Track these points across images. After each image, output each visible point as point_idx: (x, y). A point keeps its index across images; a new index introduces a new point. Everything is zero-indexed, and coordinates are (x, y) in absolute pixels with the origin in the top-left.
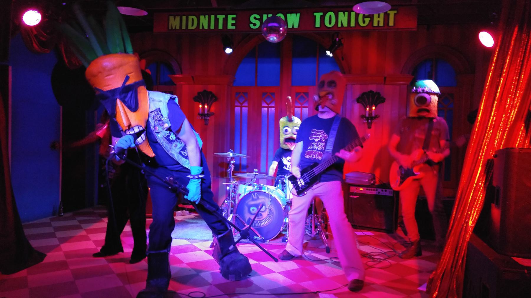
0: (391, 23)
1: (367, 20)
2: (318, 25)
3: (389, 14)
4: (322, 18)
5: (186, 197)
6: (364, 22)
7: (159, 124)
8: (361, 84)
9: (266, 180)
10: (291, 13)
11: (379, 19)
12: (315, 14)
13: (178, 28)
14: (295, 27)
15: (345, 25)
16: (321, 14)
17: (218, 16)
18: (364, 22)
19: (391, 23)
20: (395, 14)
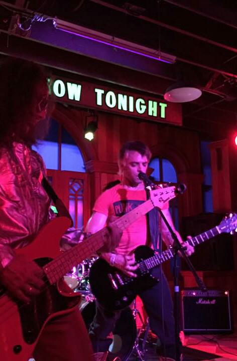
0: (163, 115)
1: (144, 108)
2: (99, 102)
3: (96, 93)
4: (104, 96)
5: (197, 303)
6: (141, 109)
7: (129, 221)
8: (108, 173)
9: (185, 287)
10: (72, 83)
11: (153, 109)
12: (96, 90)
13: (155, 115)
14: (130, 111)
15: (125, 109)
16: (103, 92)
17: (161, 104)
18: (141, 109)
19: (163, 115)
20: (165, 108)
